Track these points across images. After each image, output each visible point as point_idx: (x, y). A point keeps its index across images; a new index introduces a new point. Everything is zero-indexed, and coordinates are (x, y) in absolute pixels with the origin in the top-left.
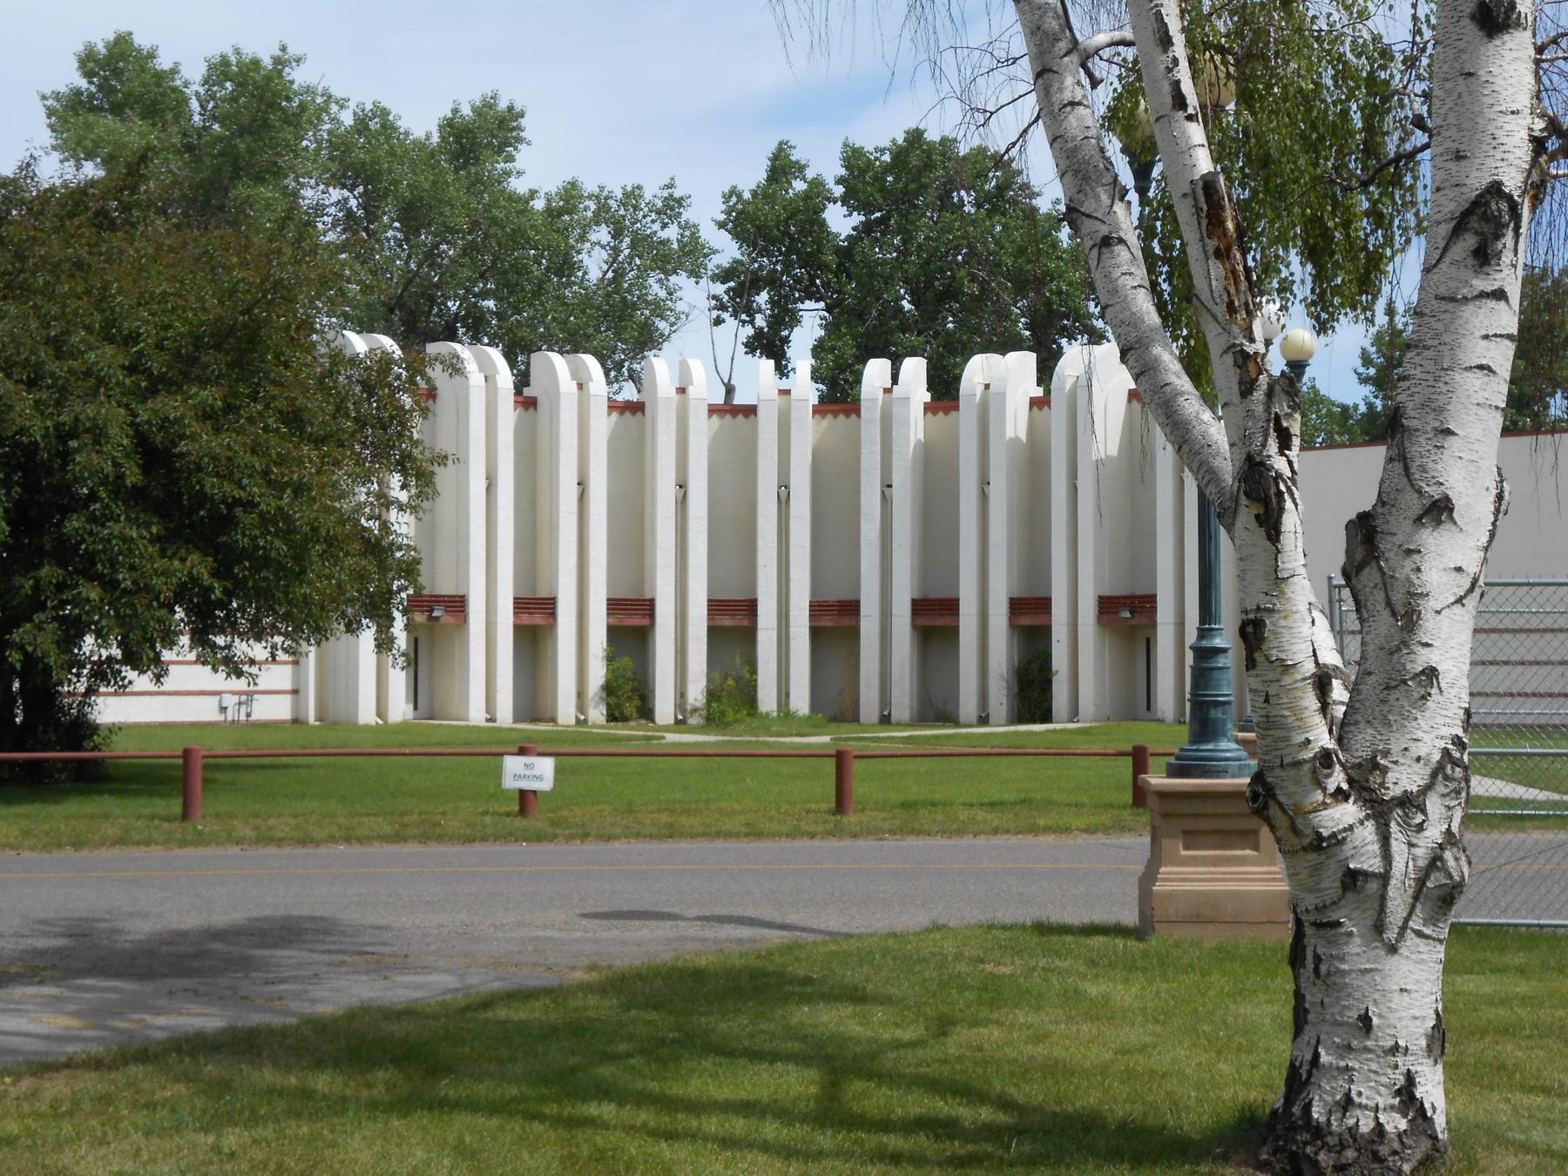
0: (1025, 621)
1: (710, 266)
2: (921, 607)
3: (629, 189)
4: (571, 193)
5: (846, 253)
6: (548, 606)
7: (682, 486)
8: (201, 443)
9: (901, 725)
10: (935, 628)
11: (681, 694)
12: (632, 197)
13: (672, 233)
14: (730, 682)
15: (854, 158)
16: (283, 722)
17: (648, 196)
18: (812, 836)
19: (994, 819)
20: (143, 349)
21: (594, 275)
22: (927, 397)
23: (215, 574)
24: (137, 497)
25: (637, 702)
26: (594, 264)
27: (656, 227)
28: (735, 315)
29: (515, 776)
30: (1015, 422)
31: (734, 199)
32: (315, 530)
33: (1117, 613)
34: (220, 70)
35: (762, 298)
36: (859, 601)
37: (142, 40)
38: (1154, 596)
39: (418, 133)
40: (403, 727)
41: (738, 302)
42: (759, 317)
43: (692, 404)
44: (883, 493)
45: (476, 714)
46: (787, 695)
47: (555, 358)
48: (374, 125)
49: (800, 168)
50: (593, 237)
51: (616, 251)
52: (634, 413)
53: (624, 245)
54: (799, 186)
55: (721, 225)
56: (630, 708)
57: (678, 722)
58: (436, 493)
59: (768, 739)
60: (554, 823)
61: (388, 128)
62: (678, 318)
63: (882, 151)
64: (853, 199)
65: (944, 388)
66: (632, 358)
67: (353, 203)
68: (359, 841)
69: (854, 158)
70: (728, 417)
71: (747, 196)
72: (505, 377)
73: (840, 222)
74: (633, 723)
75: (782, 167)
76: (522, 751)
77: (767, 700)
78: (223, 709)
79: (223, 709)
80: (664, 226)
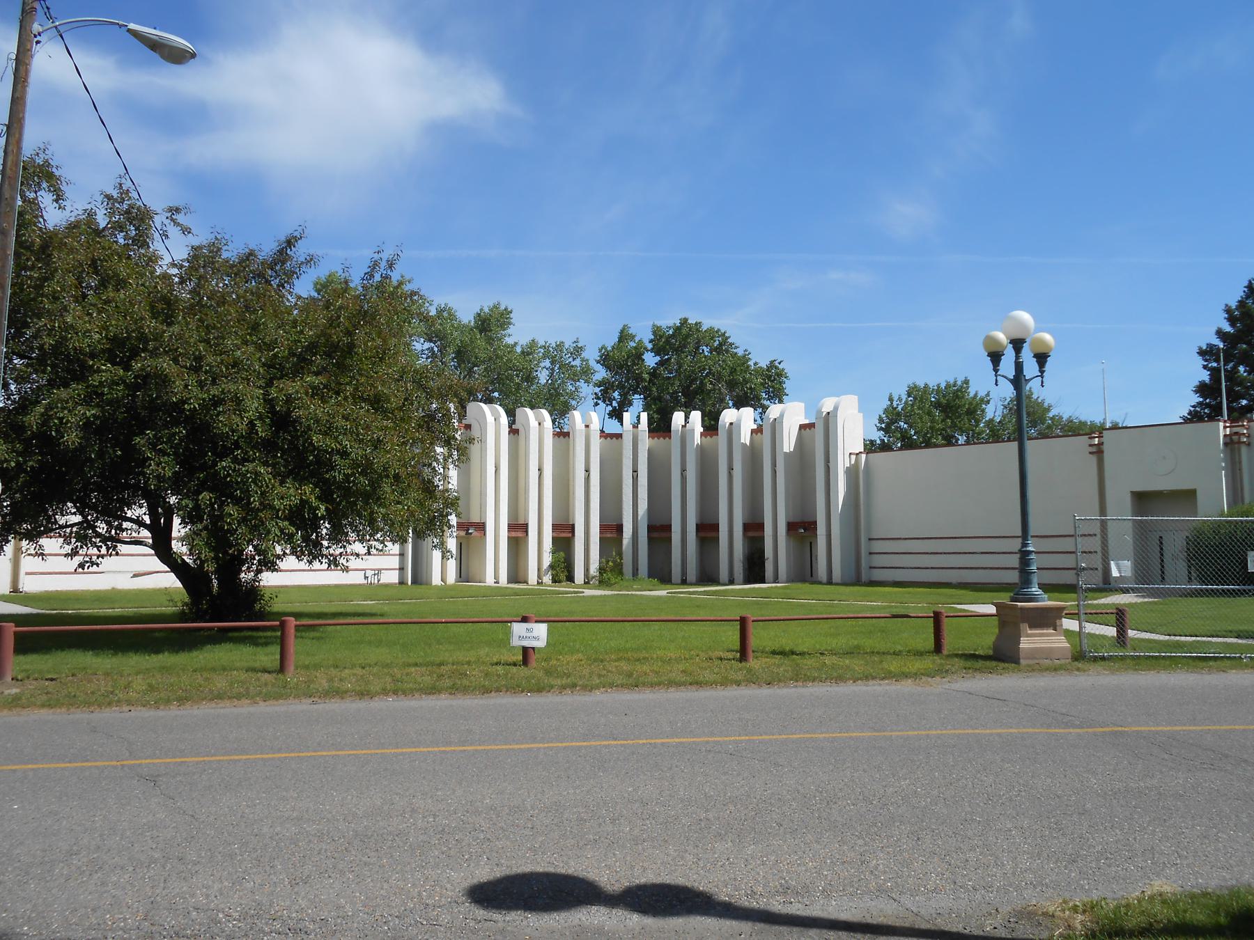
0: (751, 534)
1: (594, 379)
2: (700, 528)
4: (533, 343)
5: (654, 374)
6: (525, 528)
7: (587, 471)
8: (310, 410)
9: (691, 584)
11: (587, 570)
12: (560, 346)
13: (577, 362)
14: (610, 563)
15: (657, 331)
16: (396, 584)
17: (567, 347)
18: (738, 683)
19: (857, 665)
20: (278, 352)
21: (543, 381)
22: (702, 430)
23: (319, 498)
24: (269, 446)
25: (566, 573)
26: (543, 377)
27: (571, 359)
28: (604, 401)
29: (520, 637)
31: (603, 351)
32: (385, 469)
33: (797, 530)
35: (616, 394)
38: (816, 522)
39: (465, 321)
40: (452, 587)
41: (605, 397)
42: (614, 402)
43: (592, 433)
44: (682, 474)
45: (490, 580)
46: (637, 570)
47: (528, 410)
48: (445, 314)
49: (632, 337)
50: (542, 365)
51: (553, 369)
52: (564, 437)
53: (556, 368)
54: (633, 344)
55: (598, 362)
56: (563, 576)
57: (585, 583)
58: (468, 459)
59: (634, 593)
60: (548, 672)
61: (452, 316)
62: (581, 400)
63: (670, 328)
64: (657, 351)
65: (711, 426)
66: (560, 417)
67: (436, 349)
68: (404, 693)
69: (657, 331)
71: (609, 348)
72: (504, 419)
73: (650, 360)
74: (564, 583)
75: (624, 336)
76: (525, 620)
79: (366, 578)
80: (574, 359)
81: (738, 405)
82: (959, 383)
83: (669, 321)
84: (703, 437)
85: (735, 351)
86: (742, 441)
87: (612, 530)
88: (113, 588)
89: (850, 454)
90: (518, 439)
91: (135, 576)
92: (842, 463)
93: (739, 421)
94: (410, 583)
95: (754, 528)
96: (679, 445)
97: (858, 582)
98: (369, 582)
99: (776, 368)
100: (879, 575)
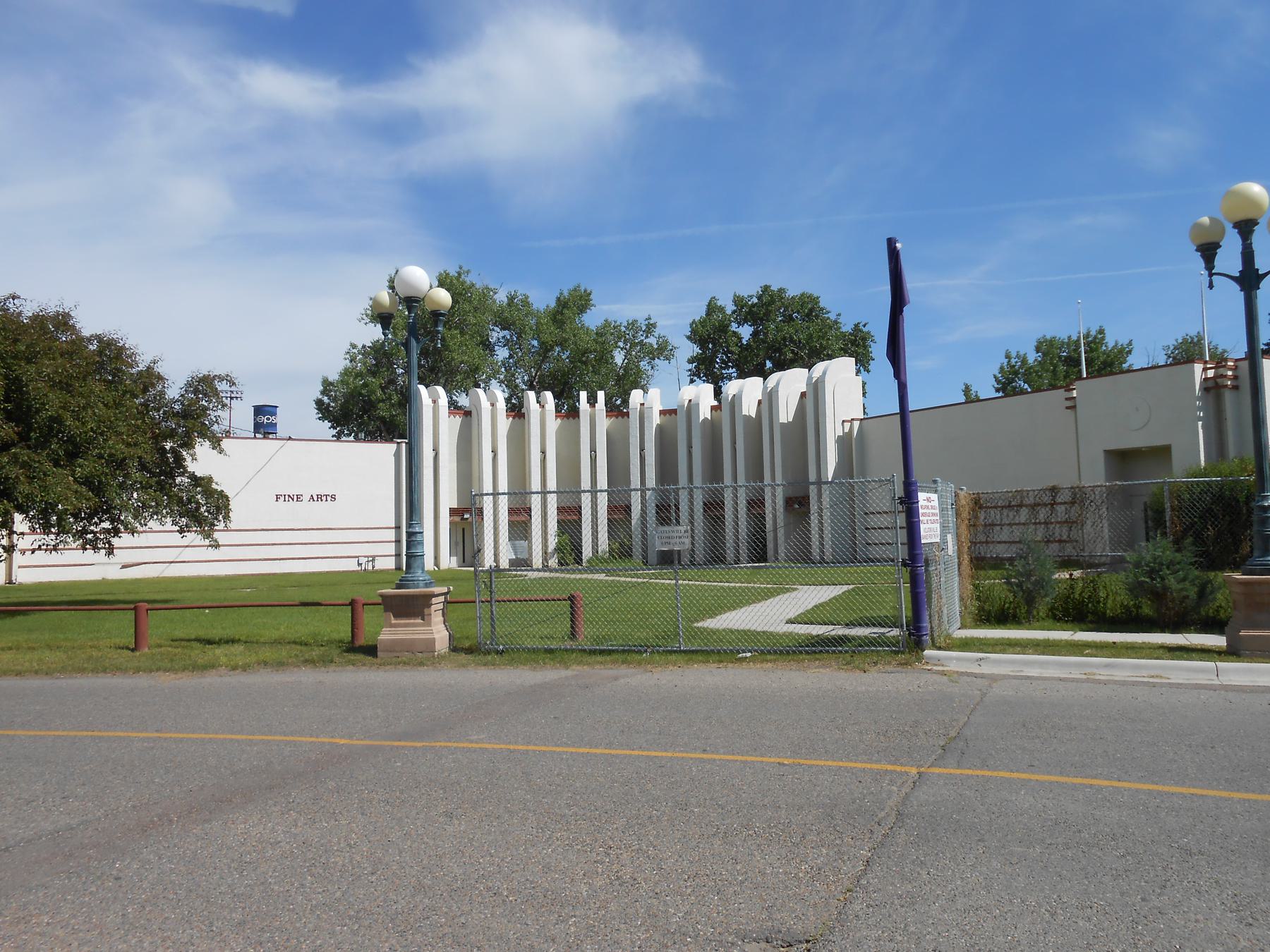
3: (630, 322)
7: (543, 452)
13: (652, 341)
15: (738, 301)
26: (619, 358)
52: (623, 417)
56: (570, 559)
61: (526, 302)
63: (751, 297)
69: (738, 301)
70: (565, 419)
75: (712, 308)
77: (587, 552)
78: (360, 564)
79: (360, 564)
81: (743, 375)
82: (1093, 333)
83: (750, 290)
84: (713, 411)
85: (826, 316)
86: (745, 412)
87: (619, 511)
88: (103, 579)
89: (843, 421)
90: (471, 421)
91: (124, 567)
92: (833, 432)
93: (698, 397)
94: (404, 569)
95: (756, 504)
96: (684, 419)
97: (854, 560)
98: (363, 568)
99: (861, 331)
100: (875, 552)
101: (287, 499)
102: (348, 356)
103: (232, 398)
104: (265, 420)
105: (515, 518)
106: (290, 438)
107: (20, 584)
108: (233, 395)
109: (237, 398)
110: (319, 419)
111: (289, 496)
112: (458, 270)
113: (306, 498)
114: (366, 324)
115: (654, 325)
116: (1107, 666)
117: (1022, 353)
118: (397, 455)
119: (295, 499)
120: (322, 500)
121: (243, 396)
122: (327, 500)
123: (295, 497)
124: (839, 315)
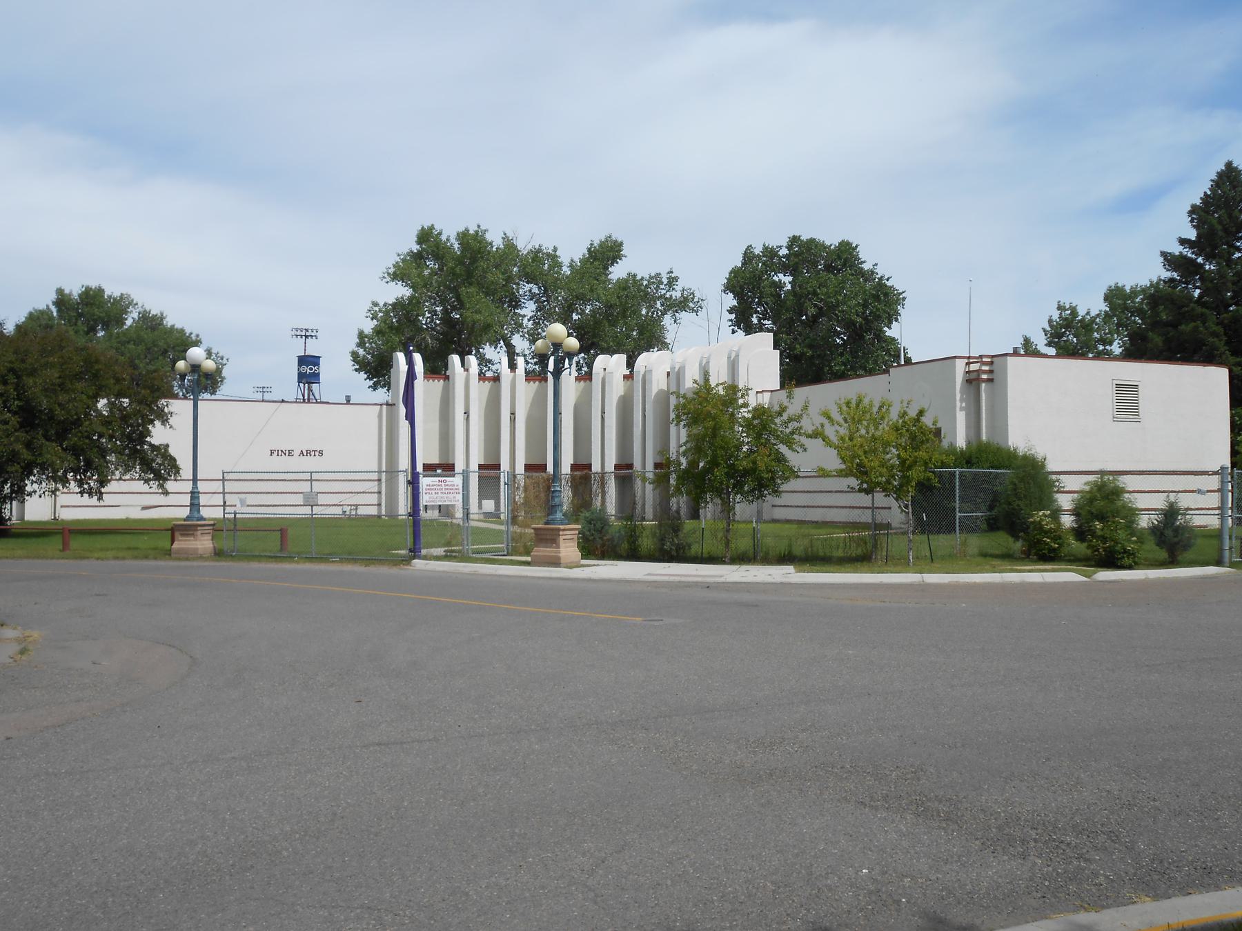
10: (381, 483)
30: (617, 387)
34: (463, 237)
36: (591, 464)
37: (438, 228)
44: (602, 416)
63: (780, 247)
89: (757, 392)
101: (280, 454)
102: (369, 314)
103: (307, 337)
104: (308, 371)
105: (486, 472)
106: (283, 401)
107: (62, 520)
108: (307, 334)
109: (312, 336)
110: (356, 370)
111: (282, 451)
112: (476, 229)
113: (297, 453)
114: (387, 282)
115: (676, 279)
116: (464, 567)
117: (1074, 305)
118: (380, 416)
119: (287, 454)
120: (310, 455)
121: (317, 334)
122: (315, 455)
123: (287, 452)
124: (876, 264)
